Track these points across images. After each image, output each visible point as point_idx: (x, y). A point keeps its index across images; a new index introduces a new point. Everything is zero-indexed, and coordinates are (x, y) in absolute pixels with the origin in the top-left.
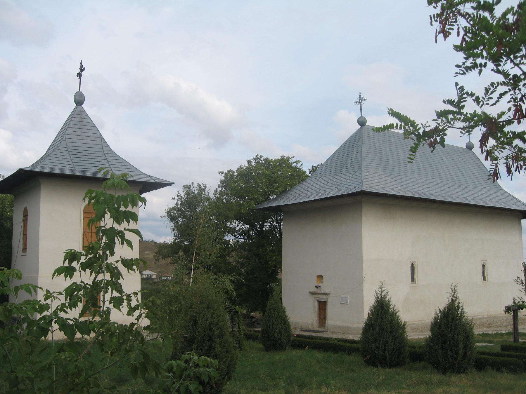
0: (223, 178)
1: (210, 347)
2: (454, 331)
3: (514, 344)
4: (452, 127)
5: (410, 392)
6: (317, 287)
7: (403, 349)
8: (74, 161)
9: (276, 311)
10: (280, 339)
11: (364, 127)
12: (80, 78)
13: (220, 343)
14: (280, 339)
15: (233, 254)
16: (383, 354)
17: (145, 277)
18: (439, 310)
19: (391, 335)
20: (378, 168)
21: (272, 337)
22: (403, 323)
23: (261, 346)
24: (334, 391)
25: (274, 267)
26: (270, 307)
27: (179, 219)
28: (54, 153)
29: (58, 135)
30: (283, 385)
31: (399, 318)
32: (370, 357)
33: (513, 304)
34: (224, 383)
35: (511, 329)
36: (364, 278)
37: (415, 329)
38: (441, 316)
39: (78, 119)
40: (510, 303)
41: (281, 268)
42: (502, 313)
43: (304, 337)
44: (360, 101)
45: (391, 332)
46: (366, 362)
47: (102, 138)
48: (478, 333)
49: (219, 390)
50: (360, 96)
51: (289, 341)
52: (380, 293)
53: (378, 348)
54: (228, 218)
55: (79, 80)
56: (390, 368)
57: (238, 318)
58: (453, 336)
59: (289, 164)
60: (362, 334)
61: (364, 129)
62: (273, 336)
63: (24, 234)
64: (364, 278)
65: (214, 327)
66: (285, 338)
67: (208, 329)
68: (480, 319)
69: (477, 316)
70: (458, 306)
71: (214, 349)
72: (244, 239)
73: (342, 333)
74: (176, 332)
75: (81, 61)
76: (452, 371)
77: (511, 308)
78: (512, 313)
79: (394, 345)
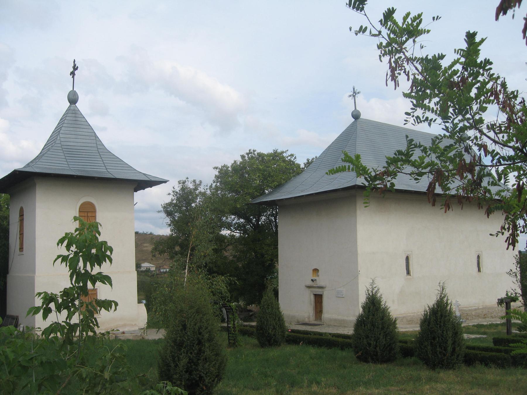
0: (217, 174)
1: (200, 350)
2: (443, 328)
3: (506, 336)
4: (402, 172)
5: (398, 389)
6: (312, 280)
7: (394, 344)
8: (68, 161)
9: (270, 307)
10: (274, 335)
11: (359, 120)
12: (73, 77)
13: (209, 347)
14: (274, 335)
15: (230, 247)
16: (375, 350)
17: (144, 270)
18: (429, 306)
19: (383, 331)
20: (372, 161)
21: (266, 333)
22: (394, 320)
23: (255, 341)
24: (324, 389)
25: (270, 261)
26: (264, 303)
27: (176, 214)
28: (49, 153)
29: (53, 135)
30: (275, 383)
31: (390, 314)
32: (362, 354)
33: (506, 297)
34: (214, 385)
37: (411, 321)
38: (430, 313)
39: (72, 118)
40: (504, 296)
41: (277, 261)
42: (495, 306)
43: (298, 332)
44: (354, 94)
45: (383, 328)
46: (358, 358)
47: (96, 136)
48: (473, 324)
49: (209, 392)
50: (354, 89)
51: (284, 337)
52: (371, 289)
53: (370, 344)
54: (223, 213)
55: (73, 78)
56: (381, 364)
57: (233, 314)
58: (442, 332)
59: (283, 157)
60: (354, 330)
61: (358, 122)
62: (267, 332)
63: (21, 233)
65: (204, 331)
66: (280, 334)
67: (197, 333)
68: (475, 310)
69: (472, 307)
70: (447, 302)
71: (204, 352)
72: (240, 233)
73: (338, 326)
74: (142, 376)
75: (74, 60)
76: (441, 367)
77: (504, 301)
78: (504, 305)
79: (385, 341)
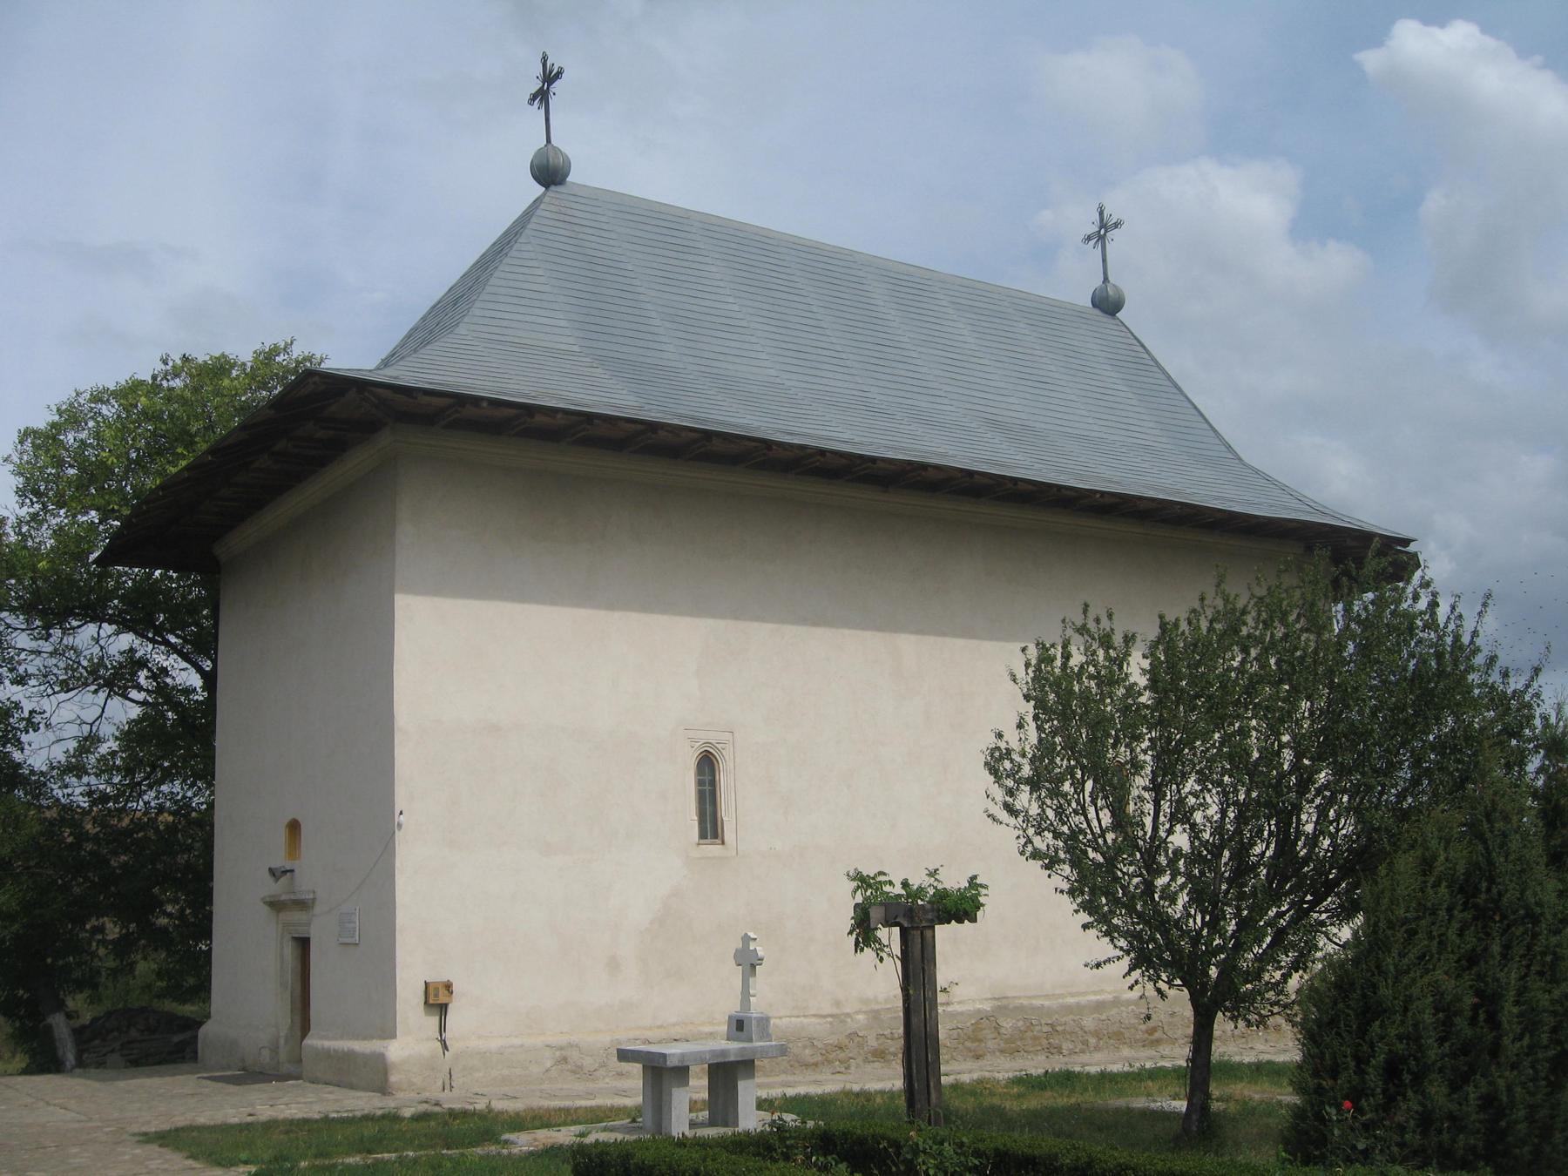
35: (888, 1079)
36: (401, 813)
50: (1101, 213)
64: (401, 813)
68: (1099, 1006)
69: (1085, 993)
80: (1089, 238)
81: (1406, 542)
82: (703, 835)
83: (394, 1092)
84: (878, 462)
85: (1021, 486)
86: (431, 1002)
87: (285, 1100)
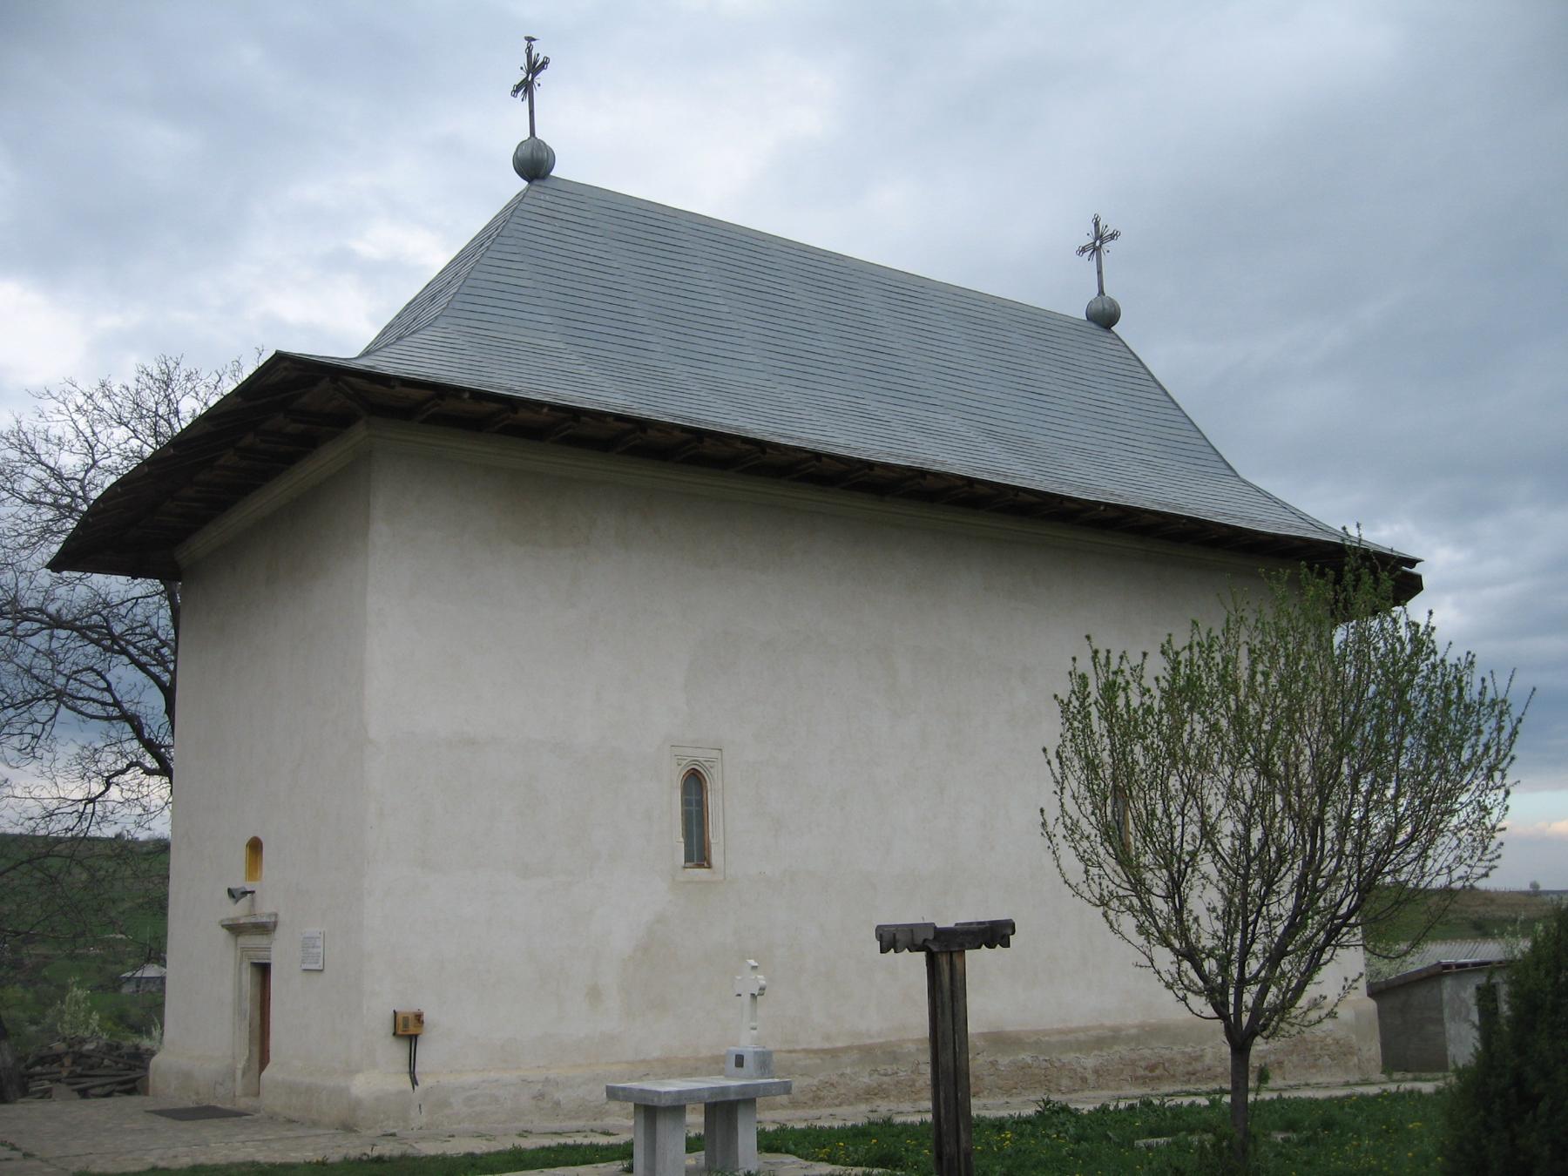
35: (916, 1110)
50: (1097, 224)
80: (1084, 250)
81: (1412, 562)
82: (689, 858)
83: (358, 1129)
84: (876, 468)
85: (1067, 504)
86: (400, 1032)
87: (242, 1137)
